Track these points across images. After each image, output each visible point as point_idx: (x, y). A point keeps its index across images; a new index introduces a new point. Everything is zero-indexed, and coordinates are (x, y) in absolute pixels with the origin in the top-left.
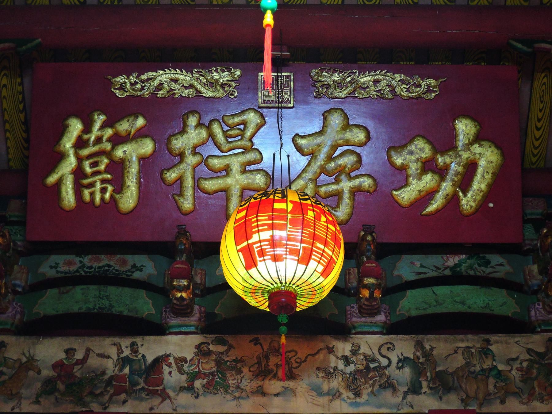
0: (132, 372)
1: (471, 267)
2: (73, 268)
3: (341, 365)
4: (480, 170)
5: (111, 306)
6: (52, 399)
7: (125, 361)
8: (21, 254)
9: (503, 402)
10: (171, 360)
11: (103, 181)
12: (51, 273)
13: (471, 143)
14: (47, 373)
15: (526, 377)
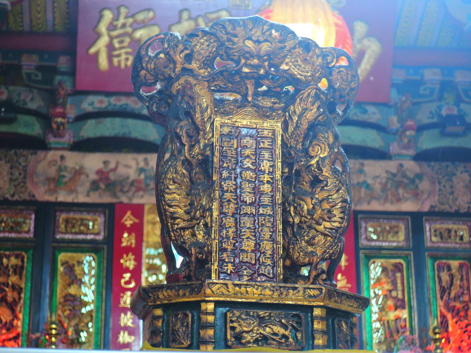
0: (146, 178)
1: (355, 114)
2: (104, 106)
4: (367, 56)
5: (130, 133)
6: (97, 193)
7: (141, 170)
8: (69, 95)
9: (369, 203)
11: (127, 53)
12: (90, 109)
13: (363, 38)
14: (93, 177)
15: (384, 188)
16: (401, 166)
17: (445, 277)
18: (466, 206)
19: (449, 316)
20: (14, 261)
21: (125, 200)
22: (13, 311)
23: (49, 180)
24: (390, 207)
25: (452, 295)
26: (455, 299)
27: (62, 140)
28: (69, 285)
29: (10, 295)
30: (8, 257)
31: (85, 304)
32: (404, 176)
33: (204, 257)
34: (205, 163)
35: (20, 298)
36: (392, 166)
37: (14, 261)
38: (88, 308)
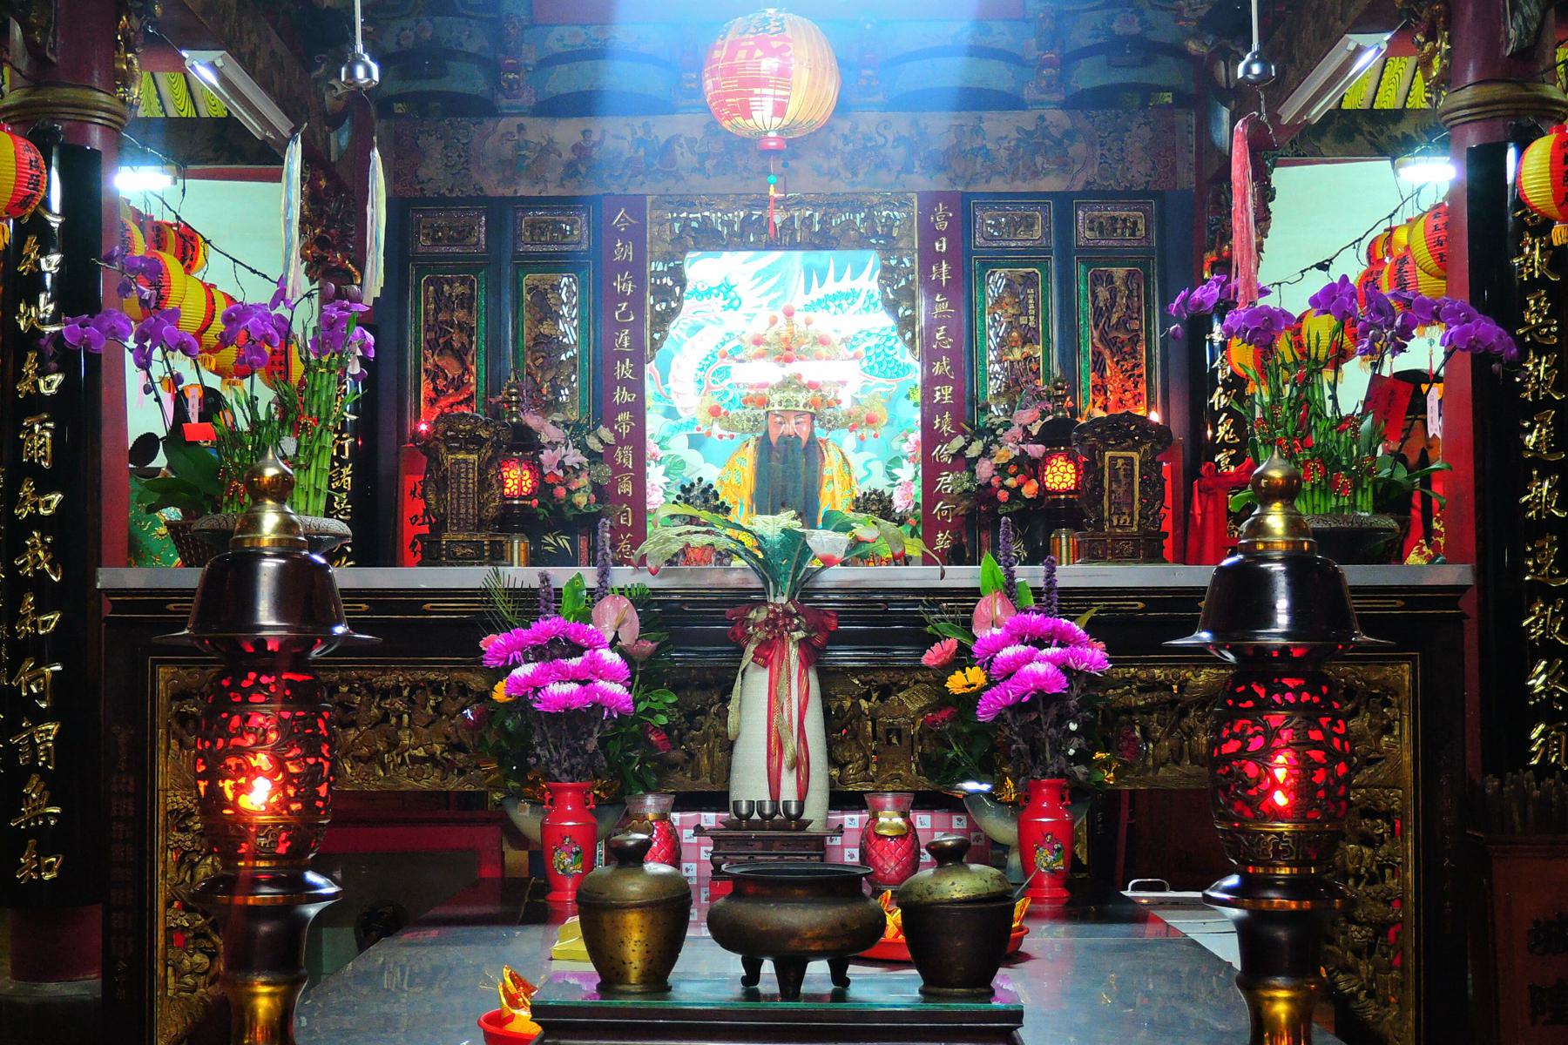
2: (578, 42)
3: (840, 144)
7: (640, 142)
9: (987, 182)
10: (682, 140)
14: (567, 156)
16: (1042, 118)
17: (1103, 293)
18: (1143, 180)
19: (1107, 353)
20: (459, 289)
21: (616, 190)
22: (462, 362)
23: (505, 163)
24: (1024, 187)
25: (1114, 320)
26: (1117, 327)
27: (519, 102)
28: (540, 321)
29: (457, 339)
30: (450, 283)
31: (566, 348)
32: (1049, 137)
33: (56, 810)
34: (444, 477)
35: (471, 343)
36: (1027, 119)
37: (459, 289)
38: (570, 354)
